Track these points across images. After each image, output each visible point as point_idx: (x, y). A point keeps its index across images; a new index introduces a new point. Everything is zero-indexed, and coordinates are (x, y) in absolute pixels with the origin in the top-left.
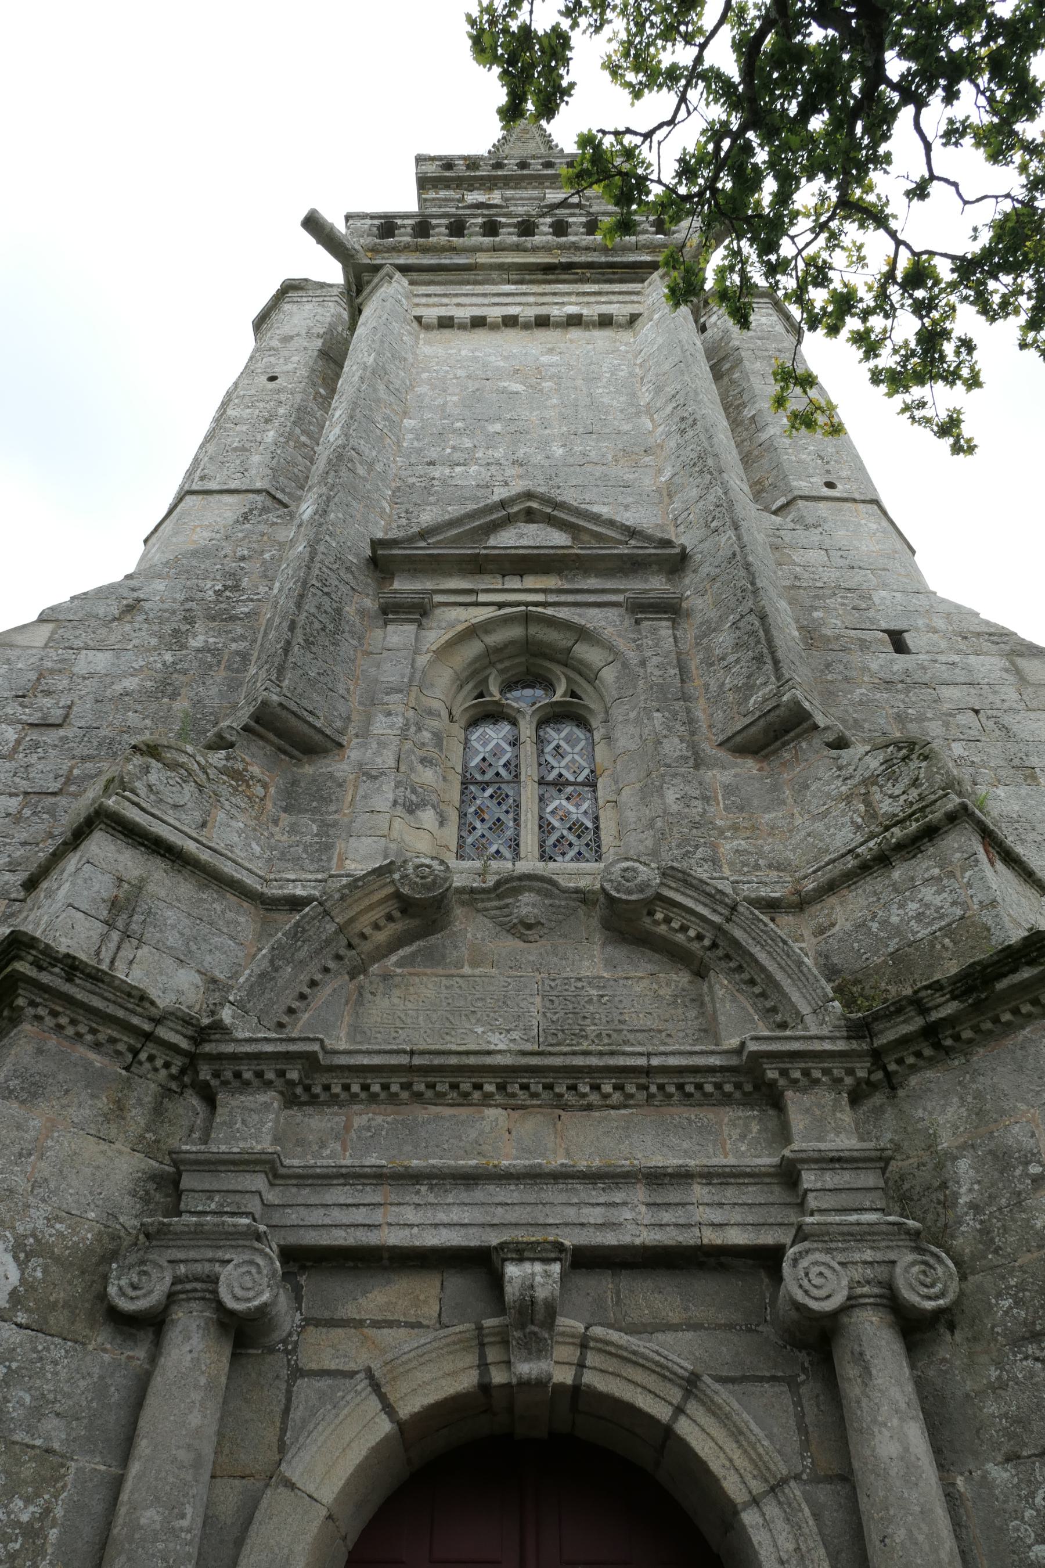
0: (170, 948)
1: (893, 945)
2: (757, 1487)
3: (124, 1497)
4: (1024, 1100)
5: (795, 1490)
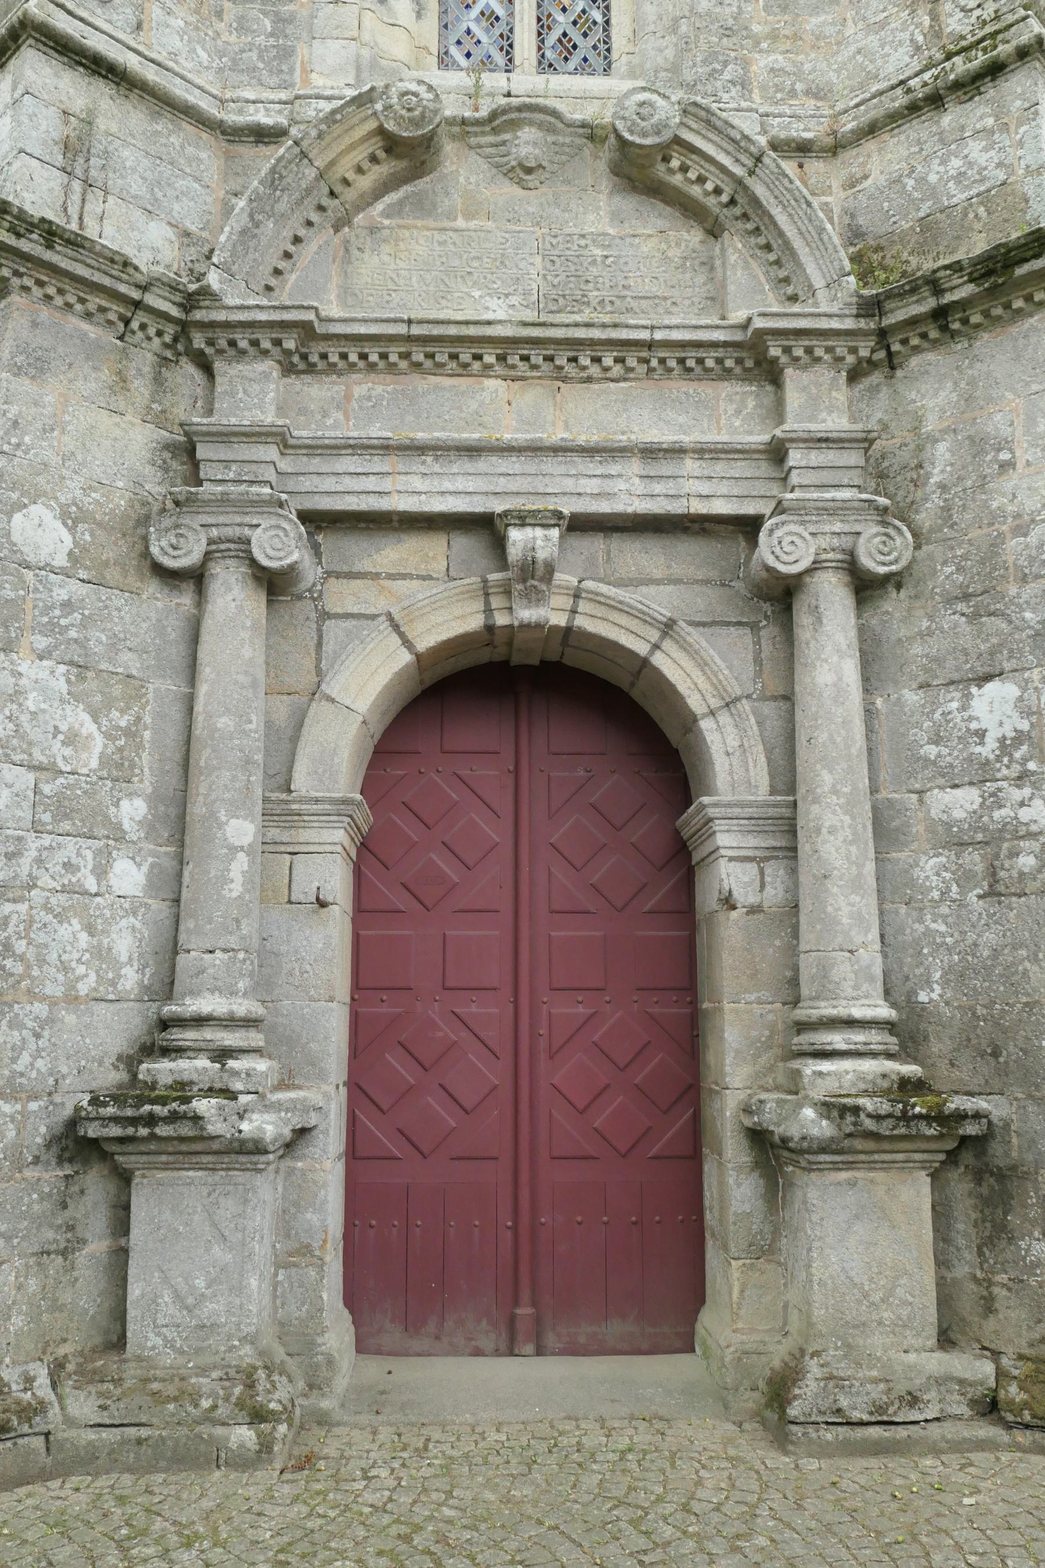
0: (135, 197)
1: (924, 210)
2: (715, 703)
3: (199, 708)
4: (1012, 390)
5: (745, 705)
